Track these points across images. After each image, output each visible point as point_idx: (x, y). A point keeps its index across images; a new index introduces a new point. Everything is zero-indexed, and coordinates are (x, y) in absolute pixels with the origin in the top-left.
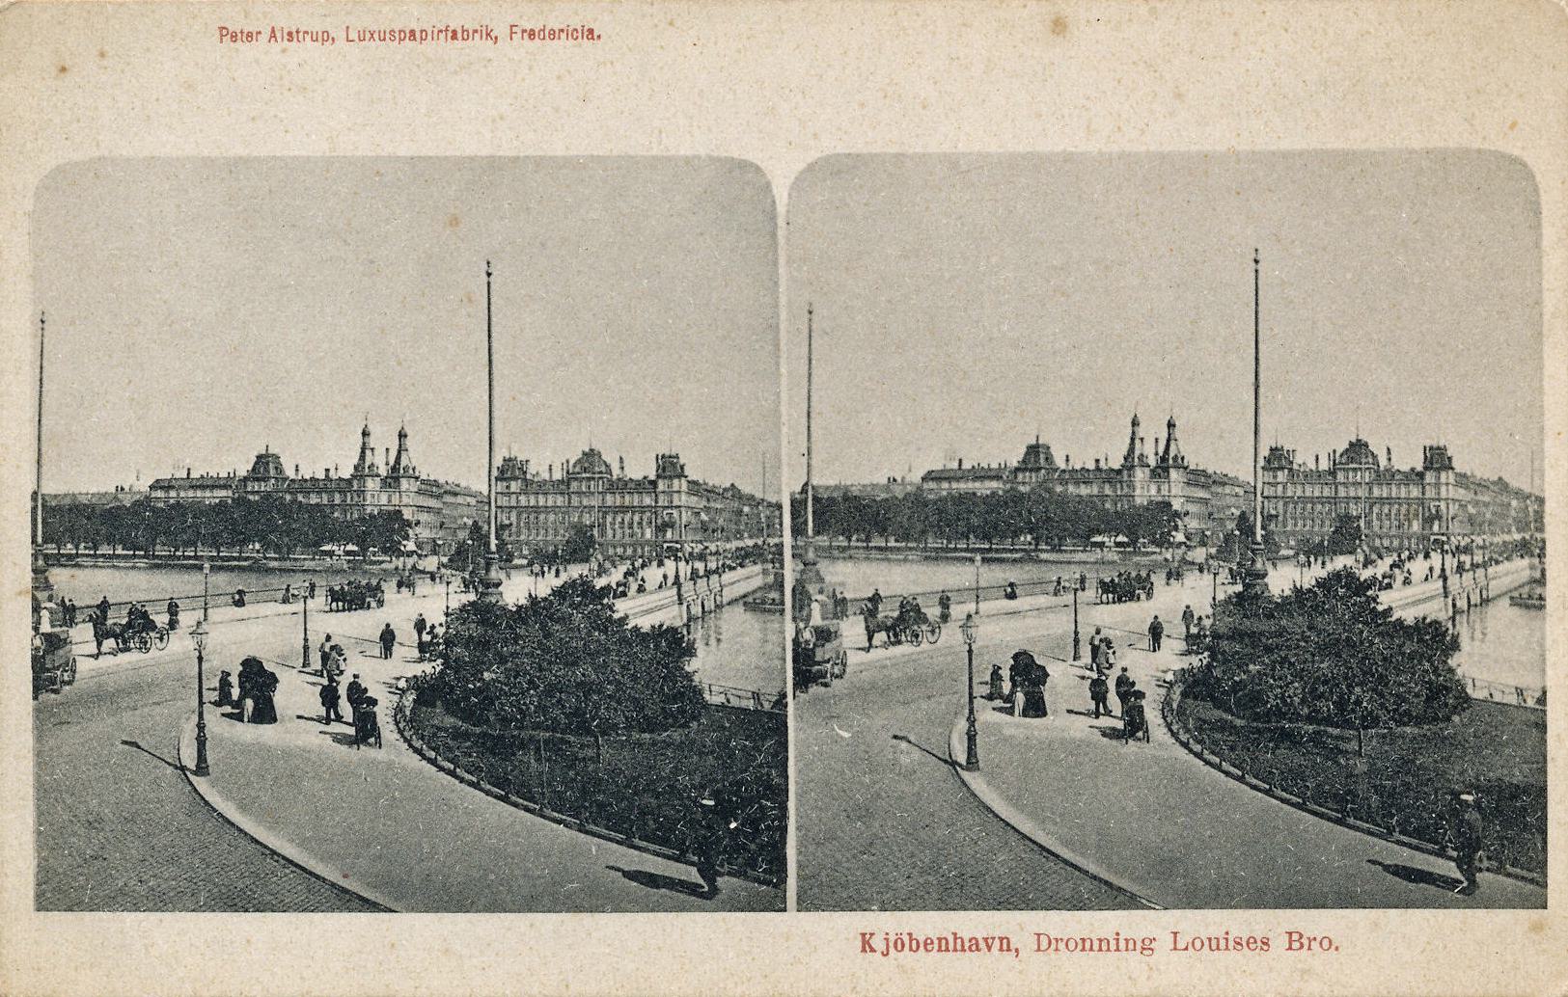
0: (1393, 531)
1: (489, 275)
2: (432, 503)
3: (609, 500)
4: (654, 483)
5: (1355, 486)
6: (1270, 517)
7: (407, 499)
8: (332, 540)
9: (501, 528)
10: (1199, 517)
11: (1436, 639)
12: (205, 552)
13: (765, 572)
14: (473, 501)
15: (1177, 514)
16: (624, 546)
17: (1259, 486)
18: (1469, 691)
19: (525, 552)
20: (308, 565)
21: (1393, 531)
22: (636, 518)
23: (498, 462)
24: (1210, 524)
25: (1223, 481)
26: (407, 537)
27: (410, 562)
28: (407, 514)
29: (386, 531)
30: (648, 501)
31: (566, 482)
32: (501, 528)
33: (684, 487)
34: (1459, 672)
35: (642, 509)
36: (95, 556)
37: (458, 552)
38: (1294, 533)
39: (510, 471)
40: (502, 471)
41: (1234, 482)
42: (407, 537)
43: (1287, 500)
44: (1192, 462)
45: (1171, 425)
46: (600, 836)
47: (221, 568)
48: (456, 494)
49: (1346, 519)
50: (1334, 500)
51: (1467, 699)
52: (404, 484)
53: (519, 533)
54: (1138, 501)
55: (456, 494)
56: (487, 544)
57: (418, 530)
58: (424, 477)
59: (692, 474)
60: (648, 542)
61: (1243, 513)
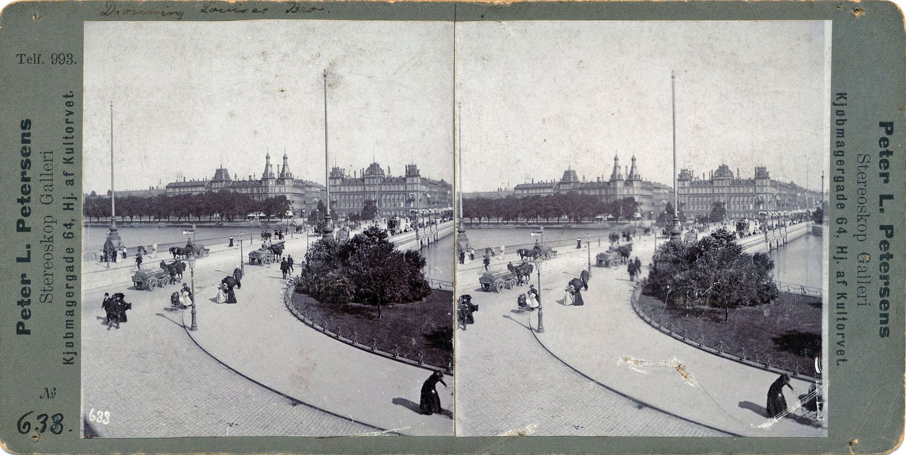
0: (392, 208)
1: (673, 77)
2: (299, 191)
3: (383, 188)
4: (404, 179)
5: (723, 190)
6: (682, 204)
7: (636, 192)
8: (252, 212)
9: (333, 203)
10: (300, 203)
11: (415, 260)
12: (192, 218)
13: (807, 226)
14: (666, 191)
15: (289, 202)
16: (740, 213)
17: (676, 189)
18: (430, 285)
19: (693, 217)
20: (243, 224)
21: (392, 208)
22: (746, 199)
23: (678, 172)
24: (653, 208)
25: (658, 187)
26: (288, 209)
27: (638, 222)
28: (637, 199)
29: (628, 208)
30: (402, 188)
31: (711, 182)
32: (333, 203)
33: (419, 181)
34: (426, 276)
35: (399, 192)
36: (141, 222)
37: (312, 215)
38: (693, 212)
39: (684, 176)
40: (681, 176)
41: (665, 187)
42: (288, 209)
43: (341, 193)
44: (296, 175)
45: (633, 160)
46: (751, 365)
47: (548, 228)
48: (659, 188)
49: (369, 203)
50: (364, 193)
51: (429, 289)
52: (635, 184)
53: (689, 208)
54: (618, 197)
55: (310, 187)
56: (326, 211)
57: (294, 205)
58: (644, 180)
59: (422, 174)
60: (751, 211)
61: (669, 203)
